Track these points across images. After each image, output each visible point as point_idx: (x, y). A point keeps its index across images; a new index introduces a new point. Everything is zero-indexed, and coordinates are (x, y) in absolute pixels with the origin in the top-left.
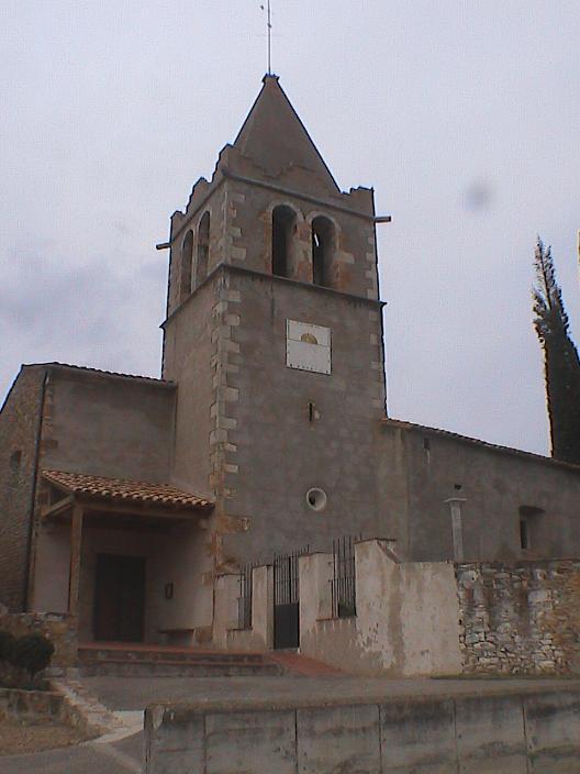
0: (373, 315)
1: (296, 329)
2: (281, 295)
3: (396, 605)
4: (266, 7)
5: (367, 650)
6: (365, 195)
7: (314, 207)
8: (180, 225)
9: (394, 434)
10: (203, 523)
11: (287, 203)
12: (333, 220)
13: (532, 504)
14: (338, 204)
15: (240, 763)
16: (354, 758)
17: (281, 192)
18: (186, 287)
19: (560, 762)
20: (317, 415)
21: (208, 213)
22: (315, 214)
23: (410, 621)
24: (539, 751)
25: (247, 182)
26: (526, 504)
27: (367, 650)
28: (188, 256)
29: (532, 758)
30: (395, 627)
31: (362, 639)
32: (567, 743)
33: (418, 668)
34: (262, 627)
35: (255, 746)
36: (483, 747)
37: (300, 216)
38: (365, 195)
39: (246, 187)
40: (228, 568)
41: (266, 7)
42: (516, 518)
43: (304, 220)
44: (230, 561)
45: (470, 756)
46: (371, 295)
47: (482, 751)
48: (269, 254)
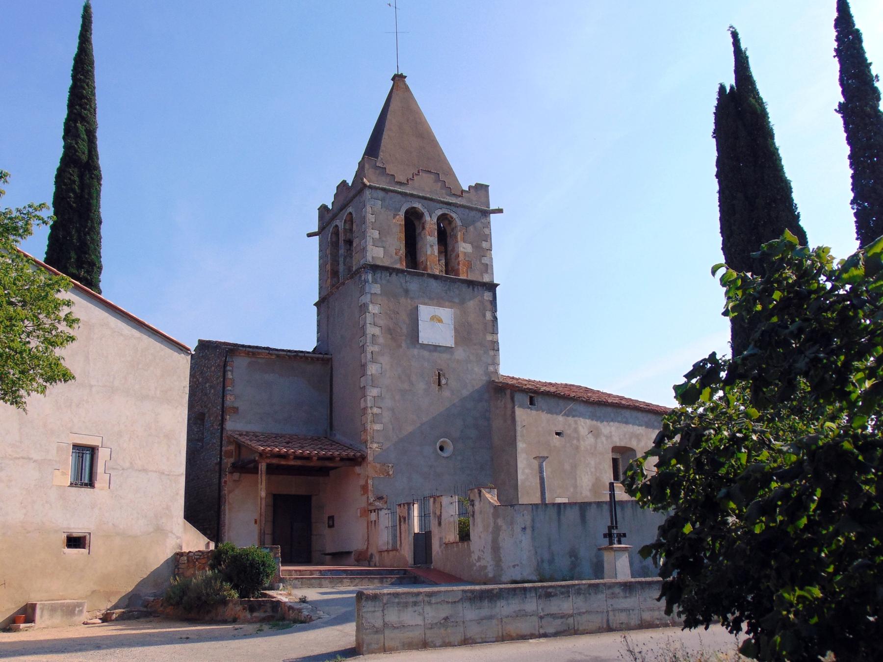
0: (487, 296)
1: (425, 312)
2: (414, 285)
3: (497, 530)
4: (393, 4)
5: (478, 564)
6: (481, 189)
7: (438, 205)
8: (328, 216)
9: (505, 394)
10: (357, 469)
11: (414, 205)
12: (454, 215)
13: (623, 444)
14: (458, 201)
15: (399, 618)
16: (451, 616)
17: (412, 195)
18: (335, 273)
19: (556, 621)
20: (443, 381)
21: (350, 213)
22: (439, 212)
23: (506, 542)
24: (544, 615)
25: (383, 190)
26: (618, 444)
27: (478, 564)
28: (335, 245)
29: (541, 618)
30: (496, 548)
31: (475, 557)
32: (561, 612)
33: (512, 576)
34: (407, 551)
35: (405, 609)
36: (514, 612)
37: (427, 218)
38: (481, 189)
39: (381, 194)
40: (378, 504)
41: (393, 4)
42: (610, 456)
43: (431, 221)
44: (380, 498)
45: (508, 616)
46: (486, 279)
47: (514, 614)
48: (403, 251)
